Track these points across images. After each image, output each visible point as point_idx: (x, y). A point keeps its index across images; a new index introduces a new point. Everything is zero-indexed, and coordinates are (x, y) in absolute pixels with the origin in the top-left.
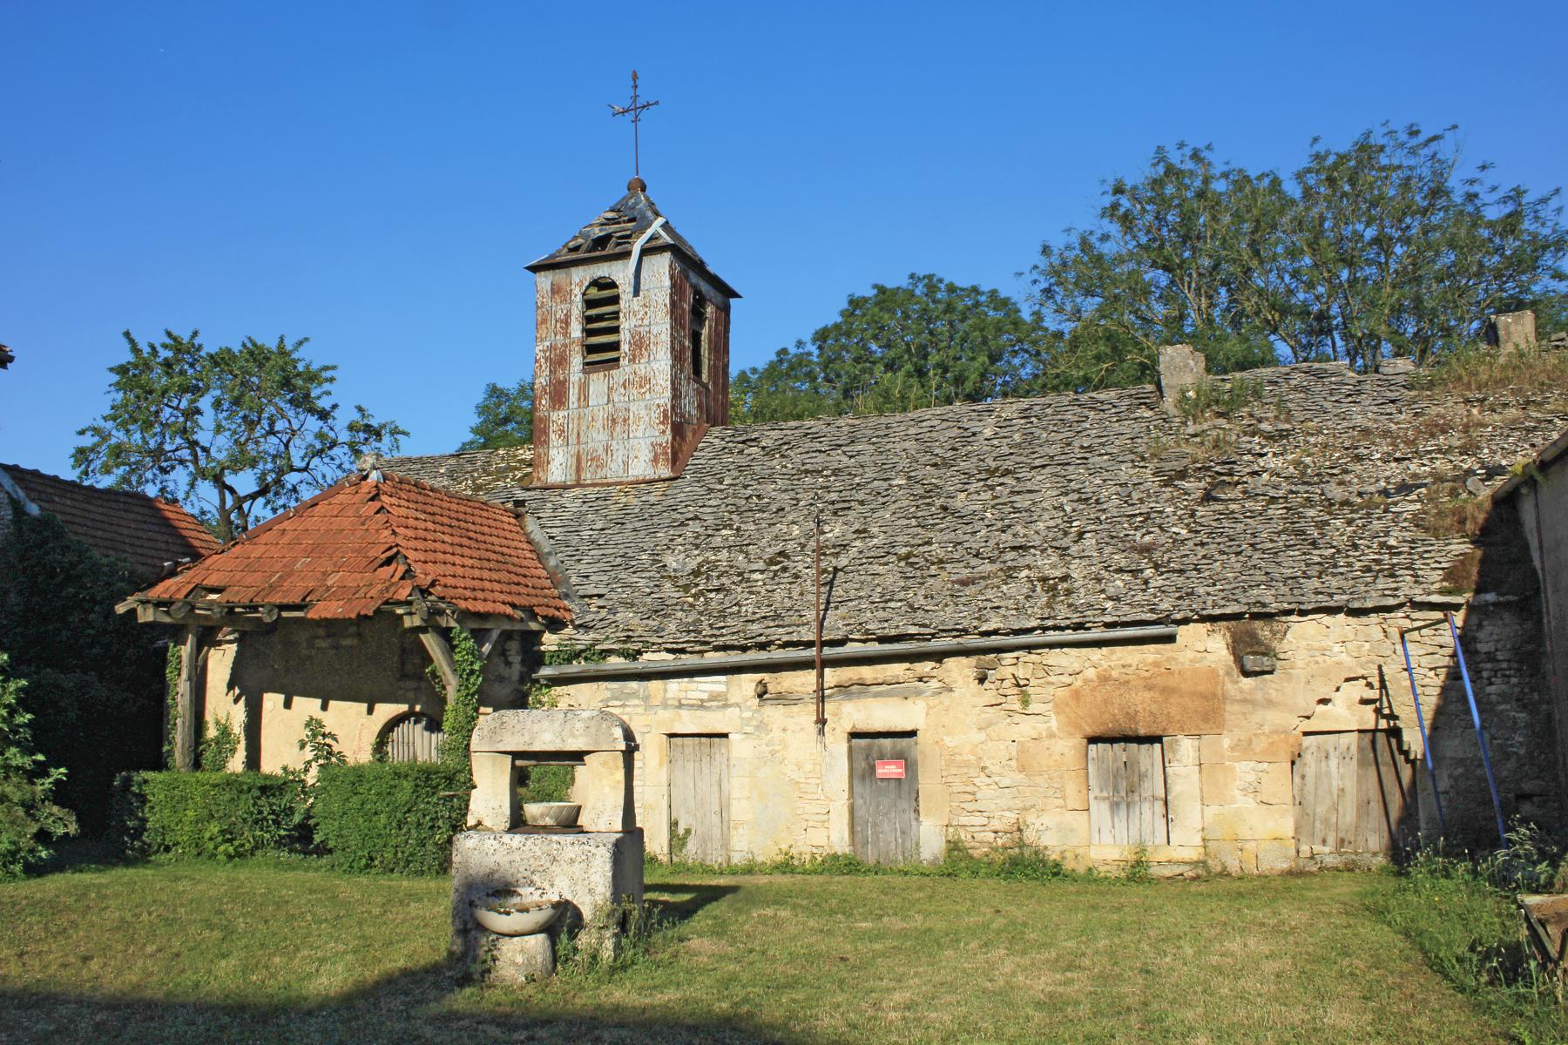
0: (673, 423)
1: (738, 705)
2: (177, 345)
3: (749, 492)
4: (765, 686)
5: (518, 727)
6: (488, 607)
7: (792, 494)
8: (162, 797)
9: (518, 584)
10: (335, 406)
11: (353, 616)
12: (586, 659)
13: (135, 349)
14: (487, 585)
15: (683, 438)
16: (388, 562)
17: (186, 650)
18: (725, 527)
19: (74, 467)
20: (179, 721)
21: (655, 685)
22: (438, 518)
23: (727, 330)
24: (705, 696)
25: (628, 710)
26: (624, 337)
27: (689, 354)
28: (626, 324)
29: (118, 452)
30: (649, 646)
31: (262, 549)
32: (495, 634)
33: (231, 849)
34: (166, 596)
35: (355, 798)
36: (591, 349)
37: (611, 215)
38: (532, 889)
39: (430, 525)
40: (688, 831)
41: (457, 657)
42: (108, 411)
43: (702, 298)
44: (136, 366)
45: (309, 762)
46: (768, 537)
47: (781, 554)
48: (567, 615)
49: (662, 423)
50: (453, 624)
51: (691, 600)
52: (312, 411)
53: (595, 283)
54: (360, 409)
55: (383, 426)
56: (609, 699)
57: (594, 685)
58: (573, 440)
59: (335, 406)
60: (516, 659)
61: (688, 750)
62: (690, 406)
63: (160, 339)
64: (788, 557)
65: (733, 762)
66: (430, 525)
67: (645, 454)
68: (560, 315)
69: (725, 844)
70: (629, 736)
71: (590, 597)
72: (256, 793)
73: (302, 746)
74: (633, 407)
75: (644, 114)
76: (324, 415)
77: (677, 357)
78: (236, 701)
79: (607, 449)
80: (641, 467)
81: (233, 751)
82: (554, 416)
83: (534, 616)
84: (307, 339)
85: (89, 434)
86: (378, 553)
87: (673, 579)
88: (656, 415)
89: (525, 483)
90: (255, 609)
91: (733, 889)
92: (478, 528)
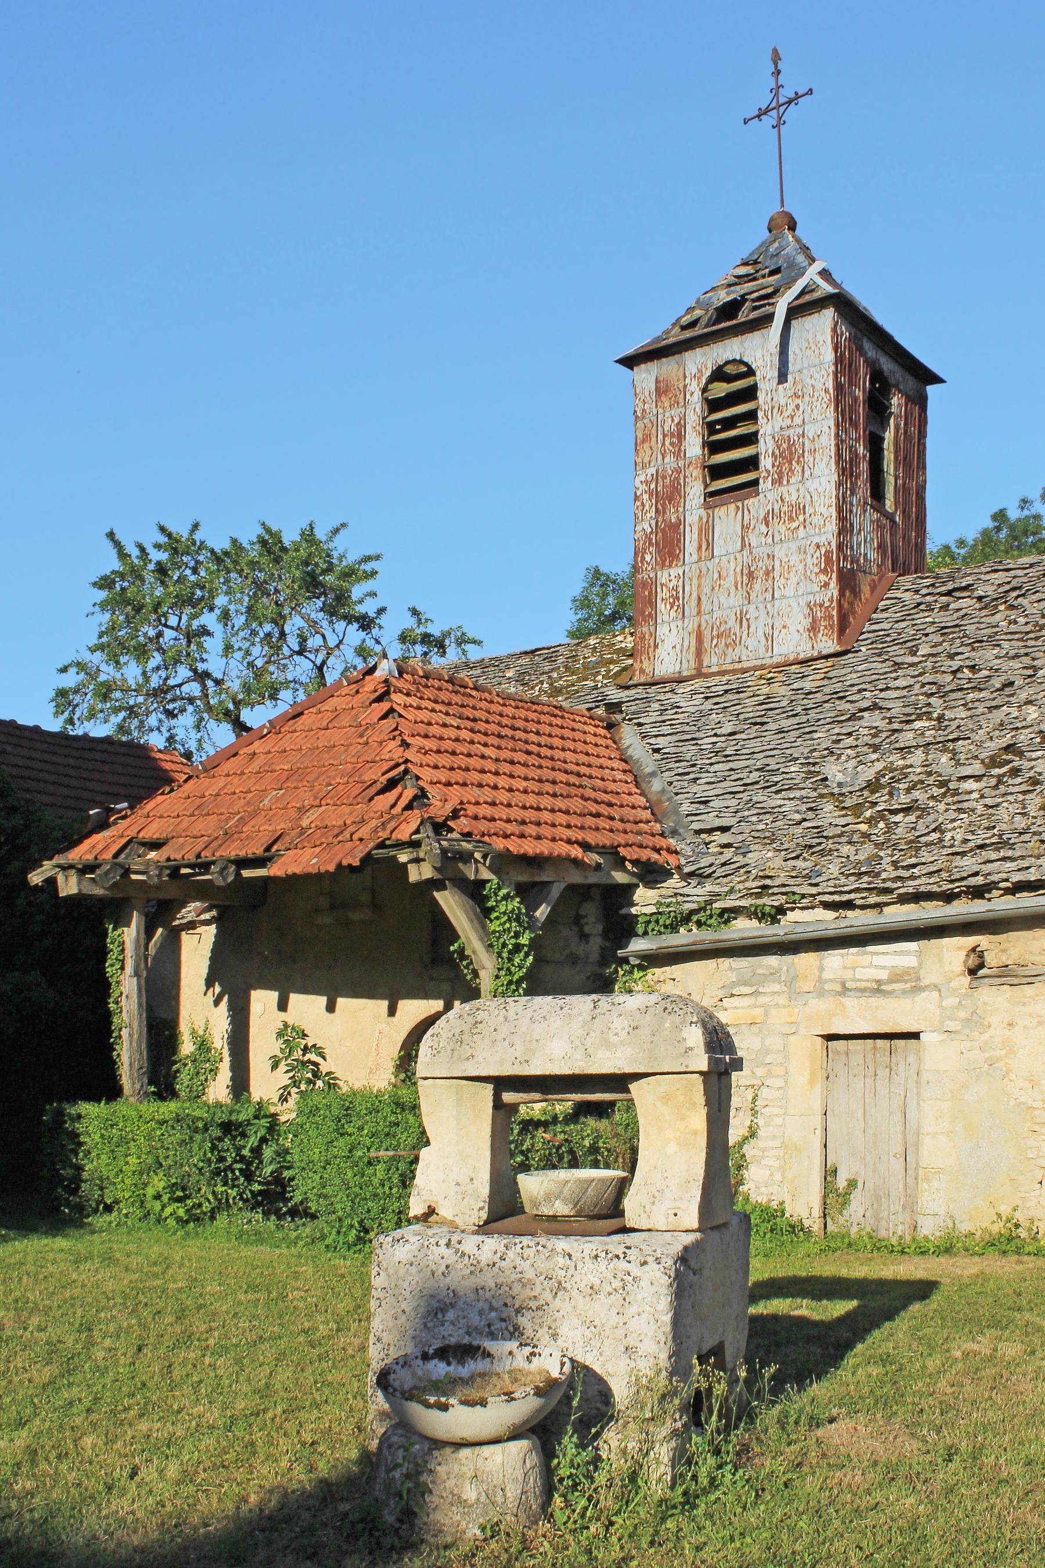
0: (840, 571)
1: (936, 987)
2: (174, 545)
3: (956, 664)
4: (981, 955)
5: (505, 1030)
6: (543, 848)
7: (1027, 660)
8: (97, 1137)
9: (598, 815)
10: (381, 611)
11: (331, 868)
12: (699, 924)
13: (123, 555)
14: (546, 816)
15: (856, 593)
16: (392, 784)
17: (130, 934)
18: (919, 718)
19: (56, 714)
20: (125, 1033)
21: (806, 960)
22: (481, 726)
23: (922, 434)
24: (884, 975)
25: (762, 1000)
26: (765, 447)
27: (864, 466)
28: (767, 428)
29: (105, 692)
30: (795, 901)
31: (221, 782)
32: (556, 891)
33: (181, 1212)
34: (90, 857)
35: (341, 1142)
36: (716, 472)
37: (743, 271)
38: (512, 1345)
39: (465, 734)
40: (852, 1184)
41: (494, 926)
42: (93, 641)
43: (885, 381)
44: (122, 576)
45: (285, 1088)
46: (987, 726)
47: (1008, 748)
48: (672, 860)
49: (824, 571)
50: (485, 874)
51: (864, 827)
52: (349, 619)
53: (719, 375)
54: (415, 612)
55: (447, 634)
56: (733, 985)
57: (711, 964)
58: (691, 609)
59: (381, 611)
60: (594, 927)
61: (856, 1060)
62: (866, 547)
63: (151, 537)
64: (1020, 754)
65: (925, 1076)
66: (465, 734)
67: (799, 620)
68: (669, 426)
69: (910, 1205)
70: (718, 1041)
71: (710, 831)
72: (217, 1132)
73: (275, 1066)
74: (780, 552)
75: (792, 113)
76: (366, 623)
77: (846, 470)
78: (217, 1002)
79: (741, 618)
80: (793, 641)
81: (215, 1071)
82: (663, 577)
83: (620, 862)
84: (344, 525)
85: (73, 671)
86: (377, 775)
87: (837, 798)
88: (814, 561)
89: (623, 680)
90: (205, 867)
91: (924, 1289)
92: (543, 740)
